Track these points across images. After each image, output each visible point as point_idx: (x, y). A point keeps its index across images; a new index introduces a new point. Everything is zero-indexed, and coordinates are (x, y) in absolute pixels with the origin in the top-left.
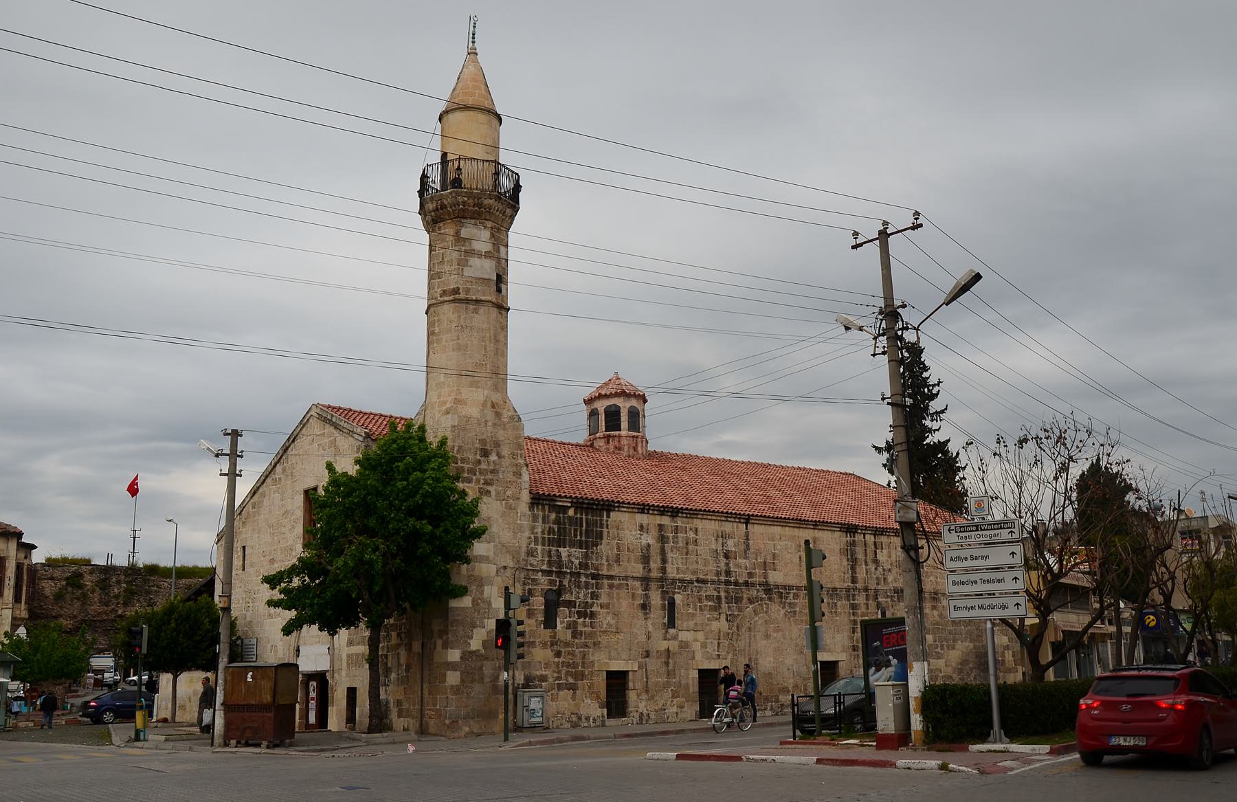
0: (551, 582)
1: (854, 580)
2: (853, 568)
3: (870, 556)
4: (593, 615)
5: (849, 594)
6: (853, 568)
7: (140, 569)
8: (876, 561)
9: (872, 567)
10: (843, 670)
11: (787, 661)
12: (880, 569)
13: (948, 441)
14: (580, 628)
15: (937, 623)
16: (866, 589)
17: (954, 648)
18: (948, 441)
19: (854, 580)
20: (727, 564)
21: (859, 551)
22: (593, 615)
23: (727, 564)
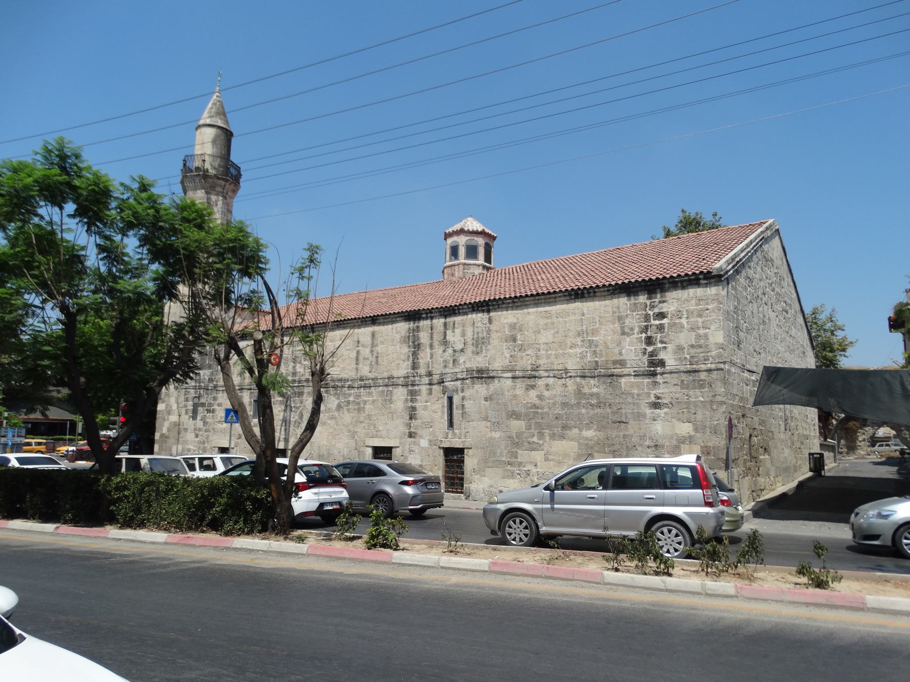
0: (196, 393)
1: (415, 366)
2: (415, 354)
3: (437, 337)
4: (213, 411)
5: (409, 384)
6: (415, 354)
7: (164, 382)
8: (445, 343)
9: (439, 350)
10: (192, 473)
11: (337, 445)
12: (450, 351)
13: (305, 249)
14: (208, 420)
15: (535, 406)
16: (430, 374)
17: (562, 437)
18: (305, 249)
19: (415, 366)
20: (294, 367)
21: (424, 337)
22: (213, 411)
23: (294, 367)
